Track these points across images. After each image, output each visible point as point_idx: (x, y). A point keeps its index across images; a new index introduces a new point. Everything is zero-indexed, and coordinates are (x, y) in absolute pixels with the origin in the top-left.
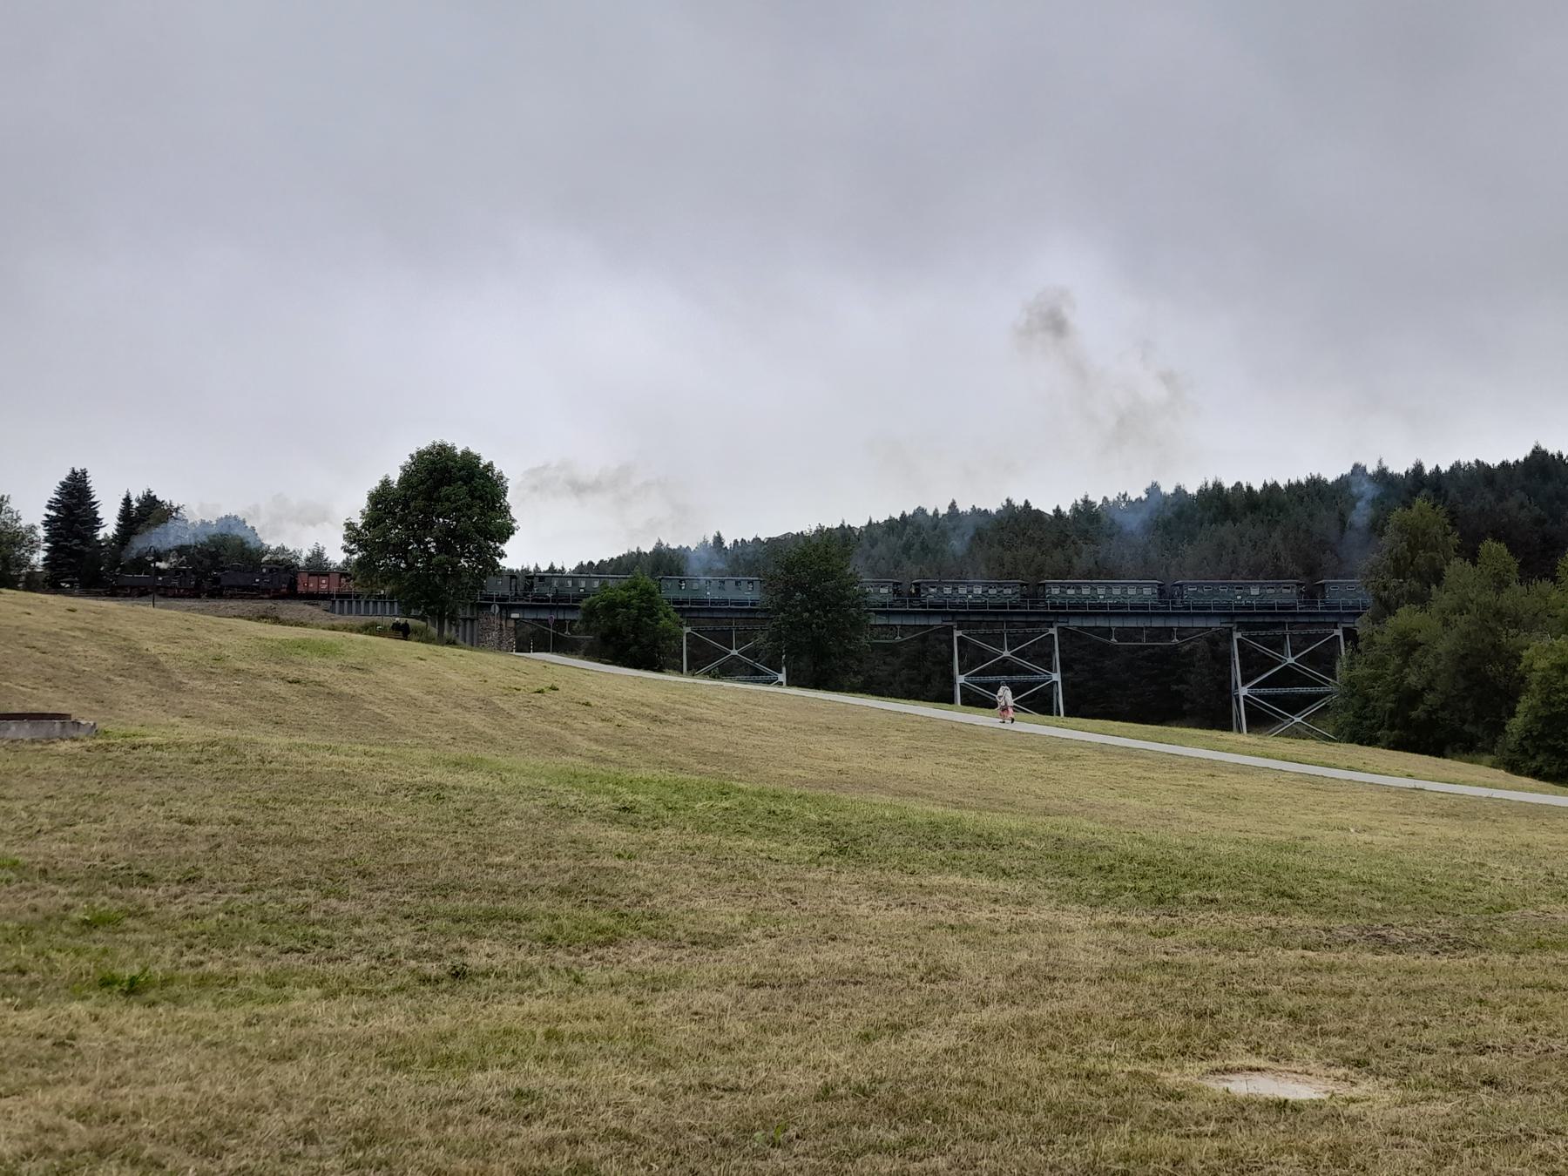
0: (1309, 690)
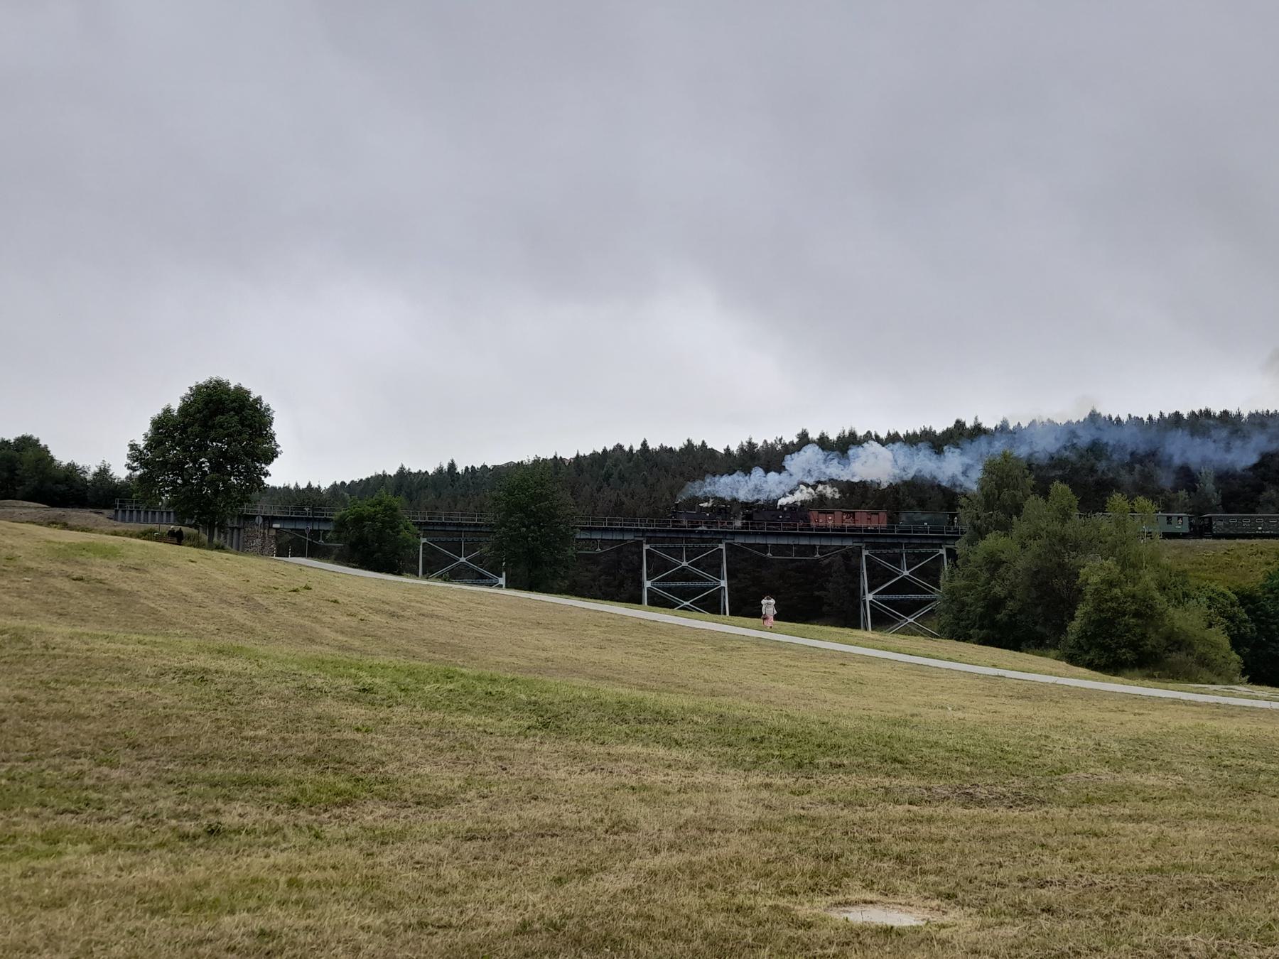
0: (673, 584)
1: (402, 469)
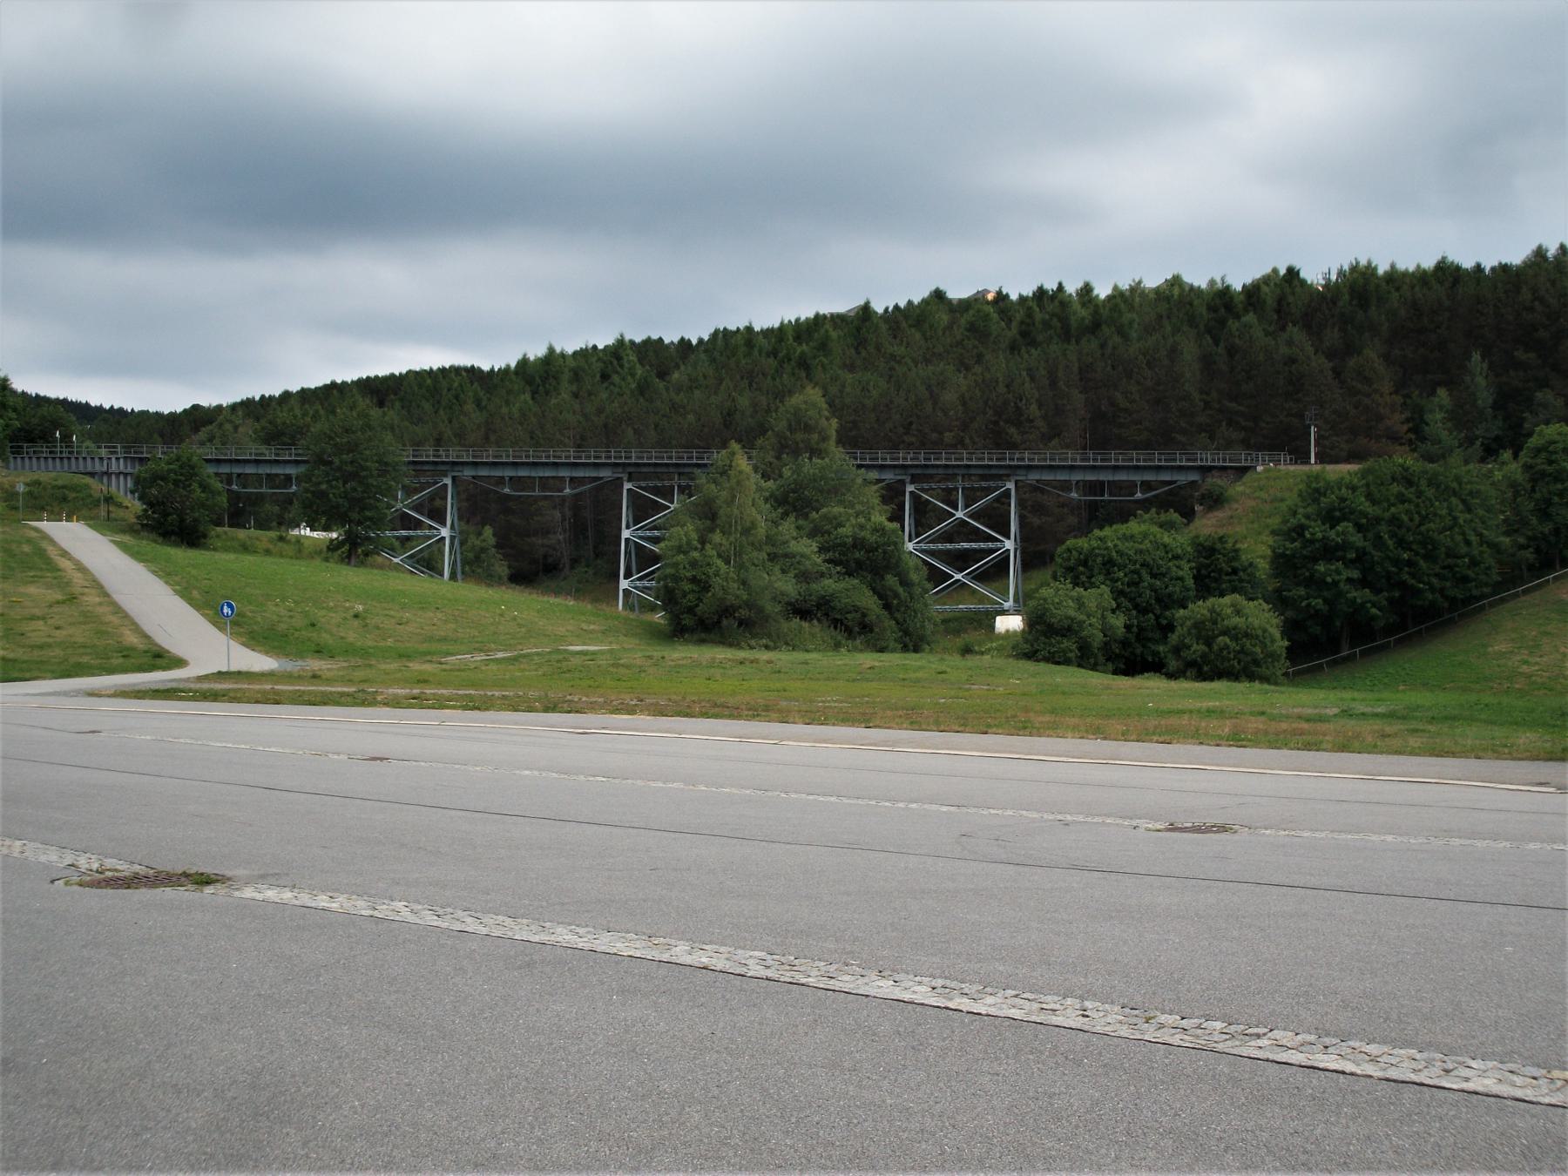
0: (982, 545)
1: (551, 350)
